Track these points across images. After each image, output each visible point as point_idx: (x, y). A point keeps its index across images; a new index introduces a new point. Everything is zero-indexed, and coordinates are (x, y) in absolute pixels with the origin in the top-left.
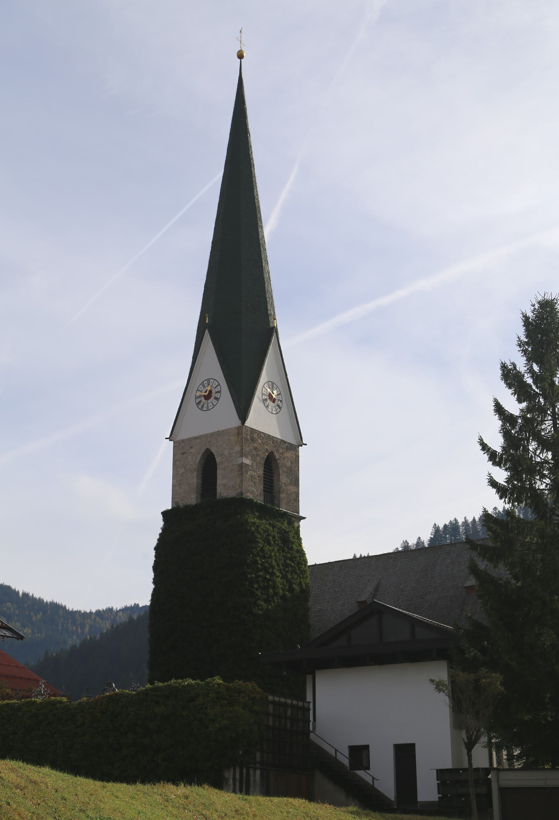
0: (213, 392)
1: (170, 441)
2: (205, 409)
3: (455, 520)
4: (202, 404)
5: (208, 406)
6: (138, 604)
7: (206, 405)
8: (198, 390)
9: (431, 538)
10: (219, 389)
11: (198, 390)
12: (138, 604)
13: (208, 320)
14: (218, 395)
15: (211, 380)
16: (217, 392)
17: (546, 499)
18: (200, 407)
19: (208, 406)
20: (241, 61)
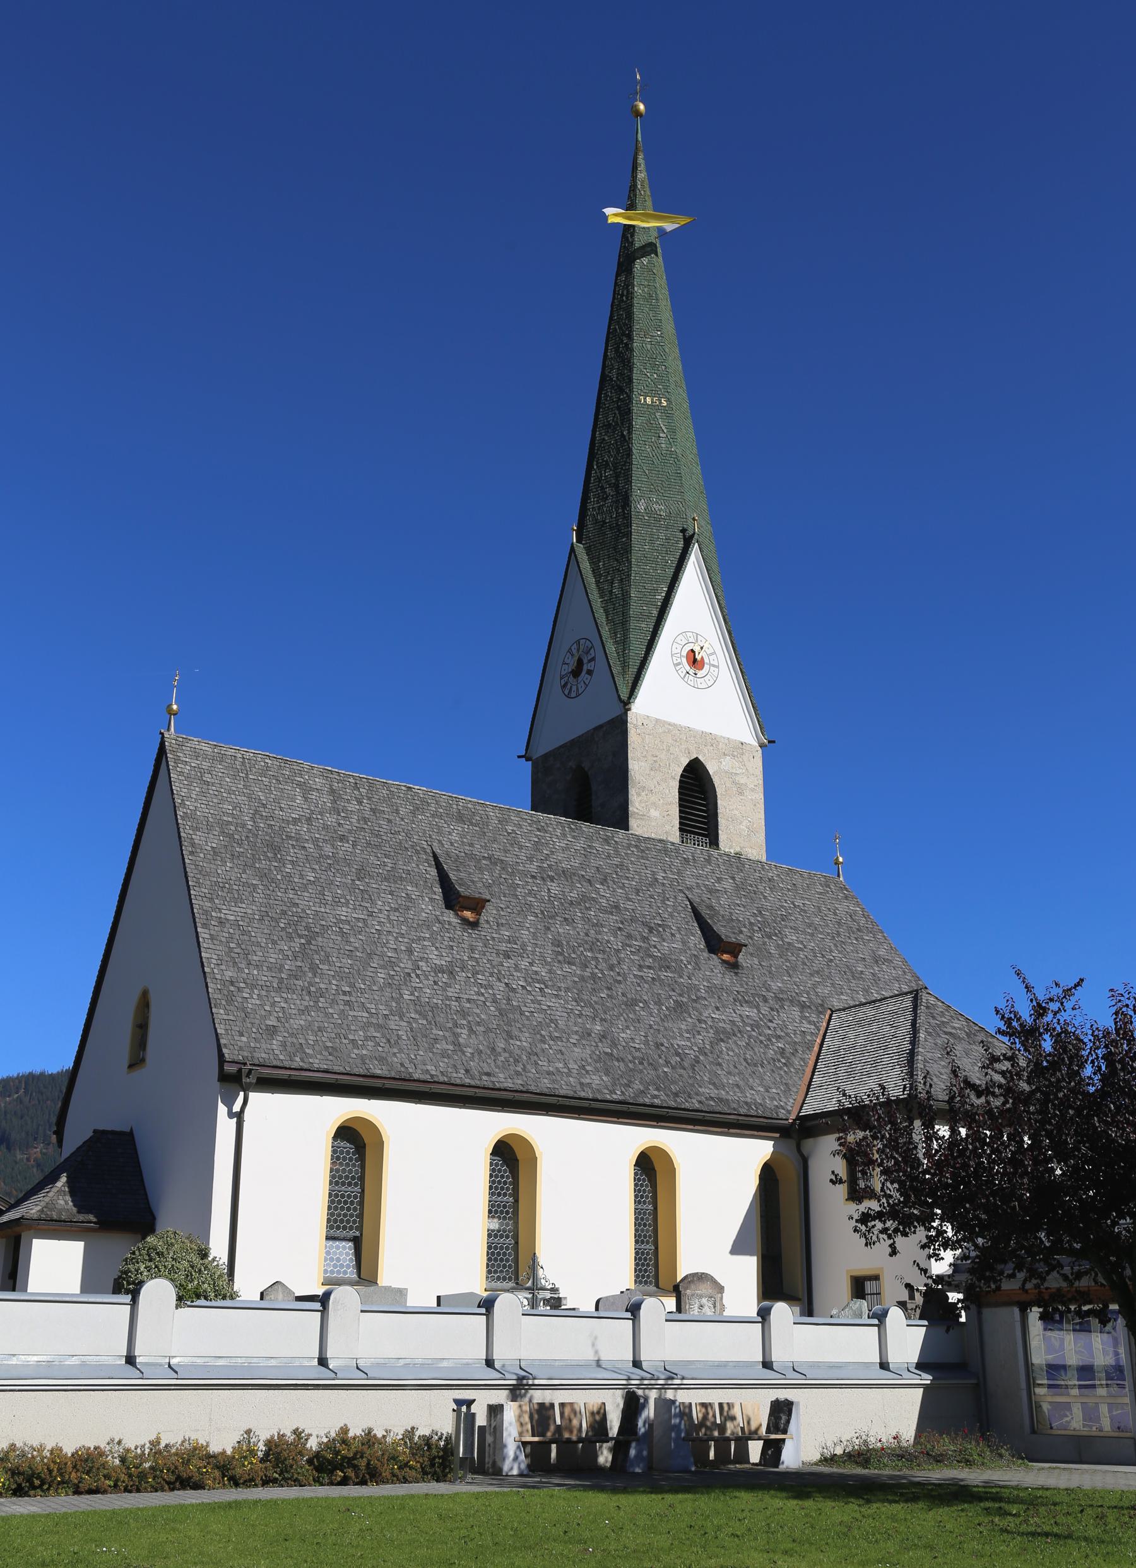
0: (585, 661)
1: (527, 760)
2: (573, 694)
3: (345, 1425)
4: (569, 686)
5: (577, 689)
6: (95, 1131)
7: (574, 688)
8: (564, 663)
9: (224, 1452)
10: (593, 655)
11: (564, 663)
12: (296, 1432)
13: (648, 170)
14: (590, 666)
15: (582, 642)
16: (590, 661)
17: (1128, 1140)
18: (566, 692)
19: (577, 689)
20: (527, 750)
